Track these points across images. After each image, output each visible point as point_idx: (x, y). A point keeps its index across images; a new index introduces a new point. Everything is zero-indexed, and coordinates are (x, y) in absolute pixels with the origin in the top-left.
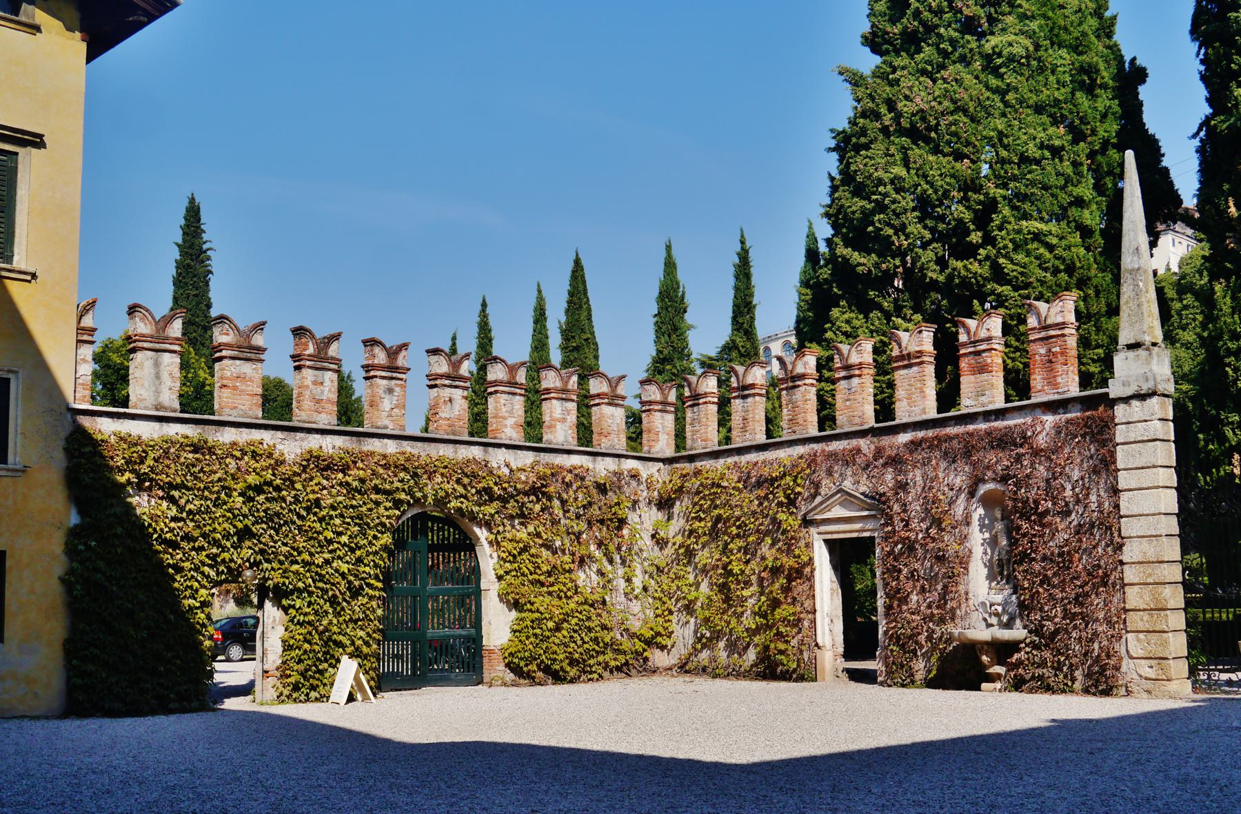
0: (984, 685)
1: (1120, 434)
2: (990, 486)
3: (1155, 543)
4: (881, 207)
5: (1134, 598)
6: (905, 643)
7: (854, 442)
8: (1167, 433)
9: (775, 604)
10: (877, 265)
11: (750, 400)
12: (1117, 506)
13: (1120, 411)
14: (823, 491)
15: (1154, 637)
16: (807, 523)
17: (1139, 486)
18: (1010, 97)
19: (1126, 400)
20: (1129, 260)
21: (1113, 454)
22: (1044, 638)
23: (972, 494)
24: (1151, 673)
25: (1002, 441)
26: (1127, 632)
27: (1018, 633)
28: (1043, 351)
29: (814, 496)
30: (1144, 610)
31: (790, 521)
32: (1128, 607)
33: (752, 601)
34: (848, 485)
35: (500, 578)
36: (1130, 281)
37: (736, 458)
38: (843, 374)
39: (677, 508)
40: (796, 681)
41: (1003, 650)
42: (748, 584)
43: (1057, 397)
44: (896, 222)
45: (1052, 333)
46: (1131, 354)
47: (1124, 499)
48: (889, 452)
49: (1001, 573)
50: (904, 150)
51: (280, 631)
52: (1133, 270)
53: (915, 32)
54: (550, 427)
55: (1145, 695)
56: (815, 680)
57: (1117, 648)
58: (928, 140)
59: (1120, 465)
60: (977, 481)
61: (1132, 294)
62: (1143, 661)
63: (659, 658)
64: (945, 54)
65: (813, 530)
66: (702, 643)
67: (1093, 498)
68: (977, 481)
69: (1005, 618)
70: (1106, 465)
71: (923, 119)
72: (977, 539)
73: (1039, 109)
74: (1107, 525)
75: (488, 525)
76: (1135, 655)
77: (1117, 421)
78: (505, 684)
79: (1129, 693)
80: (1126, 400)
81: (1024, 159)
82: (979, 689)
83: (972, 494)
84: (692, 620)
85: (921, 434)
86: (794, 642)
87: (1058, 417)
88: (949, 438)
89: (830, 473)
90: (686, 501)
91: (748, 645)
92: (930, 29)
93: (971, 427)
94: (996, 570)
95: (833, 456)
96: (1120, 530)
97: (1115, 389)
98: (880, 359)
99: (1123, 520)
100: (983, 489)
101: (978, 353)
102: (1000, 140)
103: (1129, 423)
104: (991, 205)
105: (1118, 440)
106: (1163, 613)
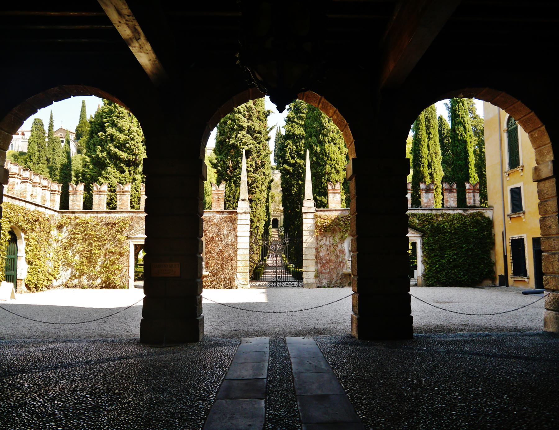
1: (239, 222)
4: (132, 139)
5: (240, 264)
8: (52, 201)
9: (113, 263)
11: (102, 196)
12: (237, 240)
13: (239, 216)
16: (128, 238)
19: (241, 213)
24: (243, 283)
28: (216, 197)
29: (131, 230)
31: (122, 237)
35: (26, 252)
37: (96, 215)
39: (64, 229)
40: (119, 288)
42: (99, 257)
44: (137, 145)
46: (243, 202)
47: (239, 239)
51: (313, 269)
57: (234, 276)
59: (238, 229)
63: (55, 283)
65: (129, 240)
66: (73, 276)
67: (230, 238)
70: (235, 229)
74: (234, 246)
75: (25, 233)
78: (25, 292)
79: (237, 288)
80: (241, 213)
84: (70, 269)
86: (119, 276)
87: (221, 216)
90: (70, 227)
91: (98, 277)
97: (238, 210)
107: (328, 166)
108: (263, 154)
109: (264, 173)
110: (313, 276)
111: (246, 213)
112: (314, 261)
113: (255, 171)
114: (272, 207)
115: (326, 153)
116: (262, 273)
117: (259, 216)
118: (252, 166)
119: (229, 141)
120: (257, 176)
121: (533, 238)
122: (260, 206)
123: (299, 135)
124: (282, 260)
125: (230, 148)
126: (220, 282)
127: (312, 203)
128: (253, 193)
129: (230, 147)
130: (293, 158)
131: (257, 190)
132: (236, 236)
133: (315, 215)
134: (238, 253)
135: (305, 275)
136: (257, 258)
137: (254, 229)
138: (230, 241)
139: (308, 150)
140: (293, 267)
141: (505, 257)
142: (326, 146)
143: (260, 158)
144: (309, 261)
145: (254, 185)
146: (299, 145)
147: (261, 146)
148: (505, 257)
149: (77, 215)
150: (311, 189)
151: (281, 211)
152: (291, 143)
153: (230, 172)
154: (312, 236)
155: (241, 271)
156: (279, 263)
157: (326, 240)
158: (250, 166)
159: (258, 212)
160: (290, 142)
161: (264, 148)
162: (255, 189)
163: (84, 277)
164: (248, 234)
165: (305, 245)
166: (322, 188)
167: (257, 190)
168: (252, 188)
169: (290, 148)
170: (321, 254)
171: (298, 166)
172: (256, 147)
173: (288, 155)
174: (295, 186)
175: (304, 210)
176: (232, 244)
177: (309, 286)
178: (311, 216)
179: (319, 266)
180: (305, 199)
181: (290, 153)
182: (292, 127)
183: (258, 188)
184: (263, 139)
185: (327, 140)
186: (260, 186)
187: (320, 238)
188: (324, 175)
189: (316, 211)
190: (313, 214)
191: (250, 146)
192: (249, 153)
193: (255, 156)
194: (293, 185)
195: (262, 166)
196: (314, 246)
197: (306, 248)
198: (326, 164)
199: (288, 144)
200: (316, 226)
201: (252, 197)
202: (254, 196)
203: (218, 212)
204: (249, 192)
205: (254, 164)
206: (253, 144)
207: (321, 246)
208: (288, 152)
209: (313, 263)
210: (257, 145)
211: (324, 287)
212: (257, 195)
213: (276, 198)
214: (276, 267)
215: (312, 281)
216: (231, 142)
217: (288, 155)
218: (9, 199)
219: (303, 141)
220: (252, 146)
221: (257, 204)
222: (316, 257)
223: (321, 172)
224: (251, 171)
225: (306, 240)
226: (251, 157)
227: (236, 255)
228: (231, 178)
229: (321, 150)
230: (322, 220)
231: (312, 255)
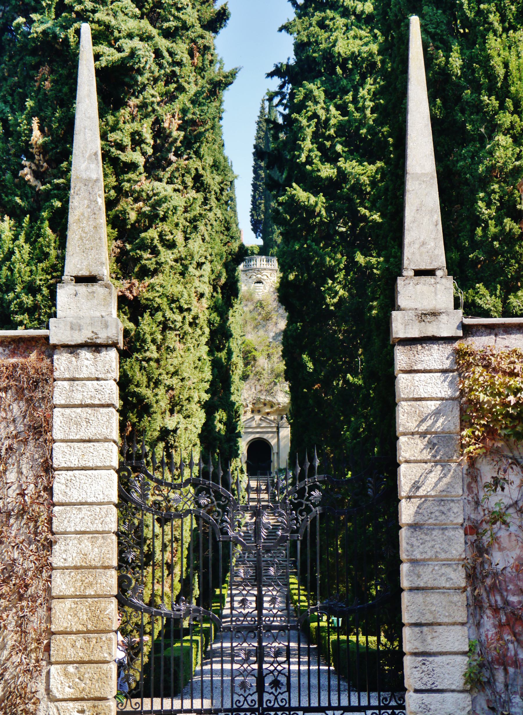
1: (60, 393)
3: (100, 541)
5: (64, 615)
12: (49, 490)
15: (88, 670)
17: (82, 464)
19: (73, 349)
20: (83, 166)
21: (48, 420)
26: (50, 663)
30: (78, 632)
32: (54, 628)
36: (83, 193)
46: (82, 288)
51: (457, 639)
52: (89, 180)
54: (278, 376)
57: (32, 686)
59: (57, 433)
61: (87, 212)
62: (71, 704)
67: (11, 476)
76: (59, 696)
77: (56, 374)
80: (73, 349)
96: (50, 521)
97: (57, 332)
99: (56, 509)
103: (73, 379)
105: (58, 400)
106: (104, 637)
107: (502, 139)
108: (192, 89)
109: (198, 178)
110: (458, 682)
111: (95, 347)
112: (460, 599)
113: (154, 167)
114: (243, 394)
115: (492, 76)
116: (197, 657)
117: (174, 381)
118: (137, 140)
119: (30, 22)
120: (163, 188)
122: (182, 338)
123: (353, 57)
124: (288, 598)
125: (30, 59)
127: (441, 292)
128: (145, 273)
129: (34, 52)
130: (330, 157)
131: (167, 256)
132: (48, 468)
133: (459, 354)
134: (59, 556)
135: (412, 672)
136: (163, 587)
137: (153, 445)
138: (13, 492)
139: (415, 21)
140: (338, 630)
141: (197, 655)
142: (494, 43)
143: (177, 106)
144: (434, 598)
145: (152, 233)
146: (355, 101)
147: (181, 48)
148: (197, 655)
150: (437, 216)
151: (280, 412)
152: (319, 94)
153: (37, 175)
154: (444, 463)
155: (71, 654)
156: (274, 609)
158: (127, 141)
159: (172, 361)
160: (317, 89)
161: (198, 59)
162: (155, 252)
164: (114, 458)
165: (407, 512)
166: (475, 245)
167: (167, 256)
168: (143, 246)
169: (315, 115)
170: (500, 560)
171: (353, 188)
172: (158, 54)
173: (307, 144)
174: (341, 276)
175: (401, 326)
176: (22, 512)
178: (438, 356)
179: (489, 624)
180: (408, 273)
181: (316, 136)
182: (322, 25)
183: (171, 245)
184: (190, 16)
185: (494, 18)
186: (179, 238)
187: (487, 471)
188: (484, 182)
189: (468, 330)
190: (448, 349)
191: (128, 45)
192: (115, 85)
193: (153, 94)
194: (331, 273)
195: (188, 143)
196: (458, 514)
197: (414, 526)
198: (494, 128)
199: (309, 96)
200: (467, 409)
201: (140, 289)
202: (152, 287)
204: (126, 265)
205: (148, 136)
206: (145, 38)
207: (497, 518)
208: (309, 132)
209: (457, 607)
210: (163, 43)
212: (167, 282)
213: (262, 361)
214: (256, 629)
216: (38, 29)
217: (307, 144)
219: (369, 86)
220: (136, 43)
221: (165, 326)
222: (472, 577)
223: (472, 167)
224: (132, 166)
225: (416, 486)
226: (133, 101)
227: (45, 567)
228: (39, 201)
229: (467, 66)
230: (499, 379)
231: (447, 563)
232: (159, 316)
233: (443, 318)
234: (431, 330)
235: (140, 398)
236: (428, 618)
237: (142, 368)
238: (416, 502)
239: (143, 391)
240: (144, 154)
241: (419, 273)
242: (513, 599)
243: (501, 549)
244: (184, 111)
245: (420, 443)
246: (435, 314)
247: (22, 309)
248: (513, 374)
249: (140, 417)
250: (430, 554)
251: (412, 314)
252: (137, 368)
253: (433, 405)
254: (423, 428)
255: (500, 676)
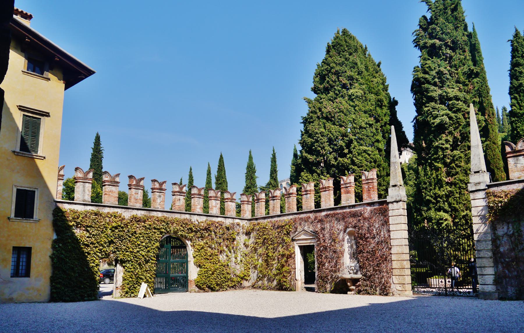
0: (348, 292)
1: (390, 213)
2: (351, 229)
4: (317, 141)
5: (395, 265)
6: (324, 279)
7: (308, 215)
9: (283, 266)
10: (315, 159)
11: (275, 201)
12: (390, 236)
14: (298, 230)
16: (293, 240)
18: (357, 108)
19: (392, 203)
21: (388, 219)
22: (368, 278)
23: (345, 232)
24: (400, 289)
25: (354, 215)
27: (359, 276)
28: (367, 187)
29: (295, 232)
31: (287, 239)
33: (275, 265)
34: (306, 228)
35: (194, 257)
37: (271, 219)
38: (305, 193)
39: (252, 235)
41: (354, 281)
42: (274, 259)
43: (371, 201)
44: (322, 146)
45: (369, 181)
46: (394, 188)
47: (392, 234)
48: (319, 218)
49: (354, 257)
50: (324, 123)
51: (490, 271)
53: (328, 87)
55: (398, 295)
56: (295, 291)
58: (331, 121)
60: (346, 227)
63: (245, 283)
64: (337, 95)
65: (295, 243)
66: (260, 278)
67: (382, 233)
68: (346, 227)
69: (355, 271)
71: (330, 114)
72: (346, 246)
73: (365, 112)
74: (386, 242)
75: (191, 240)
79: (393, 295)
80: (392, 203)
81: (361, 127)
82: (347, 294)
83: (345, 232)
85: (329, 212)
86: (289, 278)
88: (338, 214)
89: (300, 224)
90: (255, 233)
92: (332, 87)
93: (344, 211)
94: (352, 256)
95: (301, 219)
97: (389, 199)
98: (316, 189)
100: (348, 230)
101: (347, 187)
102: (354, 121)
104: (351, 141)
105: (390, 215)
112: (491, 260)
121: (18, 190)
126: (376, 287)
132: (389, 231)
133: (487, 193)
134: (393, 251)
144: (484, 260)
145: (453, 165)
147: (460, 115)
149: (259, 221)
157: (508, 229)
158: (444, 142)
163: (266, 279)
177: (486, 296)
178: (482, 194)
179: (500, 267)
190: (484, 192)
197: (478, 241)
200: (489, 208)
203: (369, 204)
210: (453, 115)
211: (511, 299)
215: (490, 288)
218: (169, 214)
222: (494, 254)
224: (447, 148)
225: (477, 230)
231: (487, 250)
232: (458, 186)
233: (482, 184)
234: (479, 187)
235: (455, 207)
236: (483, 265)
237: (454, 200)
238: (478, 234)
239: (455, 206)
240: (450, 144)
241: (475, 172)
242: (507, 260)
243: (503, 246)
244: (460, 131)
245: (478, 218)
246: (479, 183)
247: (423, 188)
248: (501, 197)
249: (455, 213)
250: (482, 248)
251: (473, 184)
252: (453, 200)
253: (481, 208)
254: (479, 214)
255: (504, 281)
